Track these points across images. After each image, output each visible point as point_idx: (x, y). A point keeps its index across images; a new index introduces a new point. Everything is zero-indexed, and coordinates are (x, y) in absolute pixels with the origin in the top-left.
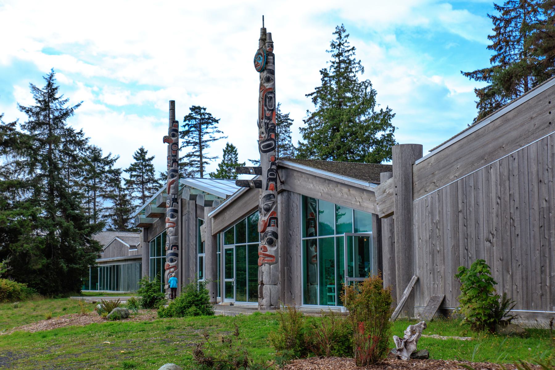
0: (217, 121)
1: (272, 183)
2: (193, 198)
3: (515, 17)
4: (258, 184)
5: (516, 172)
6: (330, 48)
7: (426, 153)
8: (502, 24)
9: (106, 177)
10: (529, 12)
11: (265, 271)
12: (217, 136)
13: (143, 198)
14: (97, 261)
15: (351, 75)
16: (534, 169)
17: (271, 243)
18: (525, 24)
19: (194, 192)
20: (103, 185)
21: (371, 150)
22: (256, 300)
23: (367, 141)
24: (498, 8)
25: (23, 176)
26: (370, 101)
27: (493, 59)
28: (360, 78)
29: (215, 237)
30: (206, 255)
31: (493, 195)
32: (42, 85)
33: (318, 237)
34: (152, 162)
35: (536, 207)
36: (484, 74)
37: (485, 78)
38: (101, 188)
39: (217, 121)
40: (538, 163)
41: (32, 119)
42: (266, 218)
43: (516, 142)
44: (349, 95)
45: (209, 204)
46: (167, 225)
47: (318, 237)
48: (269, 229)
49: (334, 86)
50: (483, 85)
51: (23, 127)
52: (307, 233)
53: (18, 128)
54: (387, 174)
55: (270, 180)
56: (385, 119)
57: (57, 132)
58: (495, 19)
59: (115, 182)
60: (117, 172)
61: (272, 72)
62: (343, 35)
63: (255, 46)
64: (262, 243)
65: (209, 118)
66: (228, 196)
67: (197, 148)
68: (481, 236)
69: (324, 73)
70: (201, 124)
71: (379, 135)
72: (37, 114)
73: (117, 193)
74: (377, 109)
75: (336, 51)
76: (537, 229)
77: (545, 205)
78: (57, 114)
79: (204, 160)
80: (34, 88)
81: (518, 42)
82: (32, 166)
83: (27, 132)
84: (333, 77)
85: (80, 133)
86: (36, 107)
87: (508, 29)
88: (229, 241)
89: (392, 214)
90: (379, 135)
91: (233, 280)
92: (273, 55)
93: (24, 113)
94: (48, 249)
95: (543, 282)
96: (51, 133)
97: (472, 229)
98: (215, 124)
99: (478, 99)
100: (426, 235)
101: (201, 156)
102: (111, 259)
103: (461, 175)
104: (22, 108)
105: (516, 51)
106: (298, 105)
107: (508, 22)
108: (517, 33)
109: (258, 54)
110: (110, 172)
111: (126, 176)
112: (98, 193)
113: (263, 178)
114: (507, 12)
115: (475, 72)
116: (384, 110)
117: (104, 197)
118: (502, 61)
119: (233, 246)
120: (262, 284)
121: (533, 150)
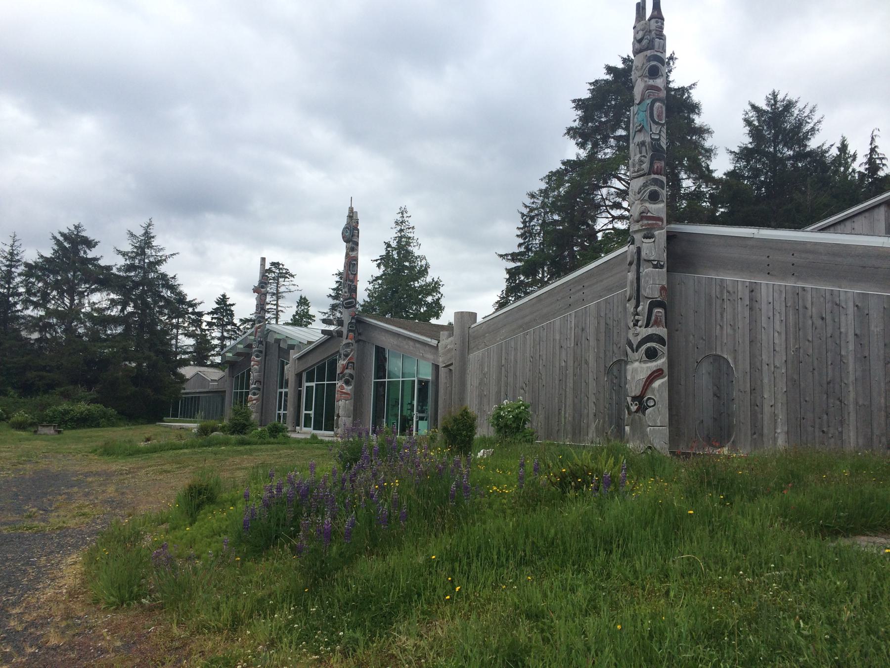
0: (292, 276)
1: (351, 334)
2: (278, 341)
3: (537, 215)
4: (340, 334)
5: (545, 339)
6: (394, 225)
7: (479, 320)
8: (527, 220)
9: (189, 317)
10: (547, 213)
11: (342, 406)
12: (292, 288)
13: (222, 338)
14: (183, 391)
15: (410, 248)
16: (557, 337)
17: (347, 383)
18: (544, 221)
19: (278, 337)
20: (186, 325)
21: (422, 310)
22: (333, 430)
23: (419, 303)
24: (526, 206)
25: (115, 312)
26: (424, 271)
27: (520, 245)
28: (417, 252)
29: (299, 376)
30: (290, 390)
31: (528, 355)
32: (139, 232)
33: (386, 380)
34: (232, 308)
35: (557, 366)
36: (514, 257)
37: (513, 260)
38: (184, 327)
39: (292, 276)
40: (561, 333)
41: (128, 262)
42: (345, 362)
43: (546, 317)
44: (407, 264)
45: (292, 347)
46: (252, 363)
47: (386, 380)
48: (347, 371)
49: (396, 256)
50: (512, 265)
51: (119, 270)
52: (377, 377)
53: (114, 271)
54: (446, 333)
55: (349, 331)
56: (435, 287)
57: (152, 275)
58: (523, 215)
59: (197, 323)
60: (200, 314)
61: (357, 244)
62: (405, 215)
63: (343, 222)
64: (339, 384)
65: (286, 273)
66: (310, 343)
67: (274, 297)
68: (518, 386)
69: (388, 245)
70: (279, 277)
71: (429, 299)
72: (133, 258)
73: (198, 332)
74: (429, 279)
75: (399, 228)
76: (557, 382)
77: (563, 364)
78: (152, 259)
79: (280, 309)
80: (132, 235)
81: (539, 234)
82: (124, 305)
83: (121, 274)
84: (395, 249)
85: (174, 278)
86: (132, 252)
87: (532, 223)
88: (310, 379)
89: (452, 364)
90: (429, 299)
91: (312, 412)
92: (358, 230)
93: (120, 256)
94: (137, 378)
95: (559, 421)
96: (144, 275)
97: (511, 380)
98: (292, 279)
99: (507, 276)
100: (476, 382)
101: (277, 305)
102: (193, 391)
103: (505, 338)
104: (119, 252)
105: (537, 242)
106: (368, 270)
107: (532, 218)
108: (539, 228)
109: (346, 228)
110: (193, 313)
111: (207, 318)
112: (180, 331)
113: (345, 330)
114: (532, 210)
115: (506, 255)
116: (436, 280)
117: (186, 335)
118: (527, 248)
119: (313, 384)
120: (338, 416)
121: (558, 323)
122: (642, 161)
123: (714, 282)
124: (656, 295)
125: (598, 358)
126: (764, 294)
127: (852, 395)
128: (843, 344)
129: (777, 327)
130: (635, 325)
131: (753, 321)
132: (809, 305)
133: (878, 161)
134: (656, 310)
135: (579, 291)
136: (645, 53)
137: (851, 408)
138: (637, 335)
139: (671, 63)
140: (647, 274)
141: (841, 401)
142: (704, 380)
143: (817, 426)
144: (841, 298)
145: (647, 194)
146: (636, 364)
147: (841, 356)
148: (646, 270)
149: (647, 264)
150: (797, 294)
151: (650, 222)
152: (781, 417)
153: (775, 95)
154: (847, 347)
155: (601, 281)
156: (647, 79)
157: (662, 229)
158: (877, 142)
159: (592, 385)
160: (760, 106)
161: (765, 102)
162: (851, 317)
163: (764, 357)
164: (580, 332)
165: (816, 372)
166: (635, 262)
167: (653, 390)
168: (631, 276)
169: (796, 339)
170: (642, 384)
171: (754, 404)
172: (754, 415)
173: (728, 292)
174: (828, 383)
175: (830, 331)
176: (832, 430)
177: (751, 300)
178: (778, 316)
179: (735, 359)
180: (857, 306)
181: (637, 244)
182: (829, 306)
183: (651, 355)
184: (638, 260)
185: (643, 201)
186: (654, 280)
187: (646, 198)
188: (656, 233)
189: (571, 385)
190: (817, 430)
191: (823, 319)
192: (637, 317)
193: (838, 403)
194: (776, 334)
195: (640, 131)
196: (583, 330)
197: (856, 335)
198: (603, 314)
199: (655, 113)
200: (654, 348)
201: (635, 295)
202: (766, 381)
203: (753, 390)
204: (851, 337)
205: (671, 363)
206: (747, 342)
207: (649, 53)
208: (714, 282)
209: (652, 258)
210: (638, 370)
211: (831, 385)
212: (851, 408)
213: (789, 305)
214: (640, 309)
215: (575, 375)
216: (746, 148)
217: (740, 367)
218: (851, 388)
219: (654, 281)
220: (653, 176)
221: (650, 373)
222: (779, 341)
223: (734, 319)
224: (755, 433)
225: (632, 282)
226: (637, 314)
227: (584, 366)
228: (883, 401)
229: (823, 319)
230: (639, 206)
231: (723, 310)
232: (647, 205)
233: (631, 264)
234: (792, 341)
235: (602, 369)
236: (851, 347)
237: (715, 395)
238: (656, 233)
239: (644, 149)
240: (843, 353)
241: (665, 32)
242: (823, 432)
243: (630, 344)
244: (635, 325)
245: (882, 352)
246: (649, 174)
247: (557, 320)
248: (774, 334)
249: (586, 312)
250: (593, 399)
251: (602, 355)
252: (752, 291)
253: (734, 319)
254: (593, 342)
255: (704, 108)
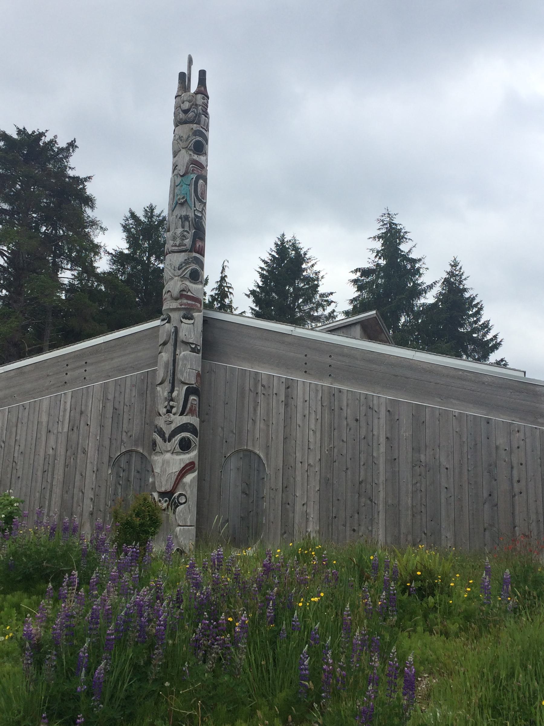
5: (25, 420)
43: (27, 394)
76: (40, 473)
77: (51, 452)
121: (45, 405)
122: (184, 236)
123: (248, 374)
124: (193, 381)
125: (99, 449)
126: (299, 392)
127: (382, 495)
128: (375, 445)
129: (313, 427)
130: (169, 411)
131: (288, 419)
132: (344, 408)
133: (226, 289)
134: (192, 398)
135: (81, 367)
136: (191, 126)
137: (381, 507)
138: (171, 422)
139: (71, 150)
140: (185, 357)
141: (371, 501)
142: (232, 477)
143: (348, 525)
144: (375, 402)
145: (188, 271)
146: (168, 456)
147: (373, 457)
148: (183, 353)
149: (184, 346)
150: (333, 394)
151: (189, 302)
152: (313, 515)
153: (152, 209)
154: (378, 450)
155: (112, 359)
156: (191, 153)
157: (200, 311)
158: (226, 273)
159: (90, 478)
160: (138, 215)
161: (143, 213)
162: (383, 421)
163: (297, 455)
164: (78, 416)
165: (349, 472)
166: (172, 342)
167: (184, 485)
168: (165, 356)
169: (330, 439)
170: (174, 478)
171: (285, 504)
172: (285, 512)
173: (263, 386)
174: (360, 483)
175: (363, 433)
176: (363, 528)
177: (287, 396)
178: (313, 416)
179: (267, 455)
180: (389, 411)
181: (174, 323)
182: (363, 409)
183: (185, 446)
184: (176, 340)
185: (183, 278)
186: (191, 365)
187: (187, 276)
188: (195, 314)
189: (61, 478)
190: (348, 529)
191: (357, 420)
192: (171, 403)
193: (369, 502)
194: (311, 432)
195: (182, 204)
196: (82, 413)
197: (387, 438)
198: (110, 397)
199: (199, 189)
200: (188, 438)
201: (169, 378)
202: (298, 478)
203: (285, 488)
204: (382, 440)
205: (200, 455)
206: (281, 438)
207: (195, 126)
208: (248, 374)
209: (191, 341)
210: (169, 462)
211: (363, 484)
212: (381, 507)
213: (324, 404)
214: (175, 394)
215: (66, 466)
216: (121, 253)
217: (273, 465)
218: (381, 488)
219: (189, 365)
220: (194, 254)
221: (182, 465)
222: (314, 439)
223: (268, 415)
224: (285, 533)
225: (167, 365)
226: (172, 400)
227: (80, 455)
228: (410, 501)
229: (357, 420)
230: (180, 283)
231: (256, 404)
232: (188, 283)
233: (165, 344)
234: (326, 439)
235: (106, 459)
236: (382, 449)
237: (243, 492)
238: (195, 314)
239: (187, 224)
240: (375, 454)
241: (209, 110)
242: (354, 530)
243: (161, 433)
244: (169, 411)
245: (410, 455)
246: (191, 251)
247: (45, 400)
248: (309, 432)
249: (88, 392)
250: (89, 494)
251: (107, 443)
252: (288, 388)
253: (268, 415)
254: (94, 428)
255: (98, 203)
